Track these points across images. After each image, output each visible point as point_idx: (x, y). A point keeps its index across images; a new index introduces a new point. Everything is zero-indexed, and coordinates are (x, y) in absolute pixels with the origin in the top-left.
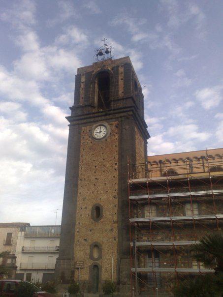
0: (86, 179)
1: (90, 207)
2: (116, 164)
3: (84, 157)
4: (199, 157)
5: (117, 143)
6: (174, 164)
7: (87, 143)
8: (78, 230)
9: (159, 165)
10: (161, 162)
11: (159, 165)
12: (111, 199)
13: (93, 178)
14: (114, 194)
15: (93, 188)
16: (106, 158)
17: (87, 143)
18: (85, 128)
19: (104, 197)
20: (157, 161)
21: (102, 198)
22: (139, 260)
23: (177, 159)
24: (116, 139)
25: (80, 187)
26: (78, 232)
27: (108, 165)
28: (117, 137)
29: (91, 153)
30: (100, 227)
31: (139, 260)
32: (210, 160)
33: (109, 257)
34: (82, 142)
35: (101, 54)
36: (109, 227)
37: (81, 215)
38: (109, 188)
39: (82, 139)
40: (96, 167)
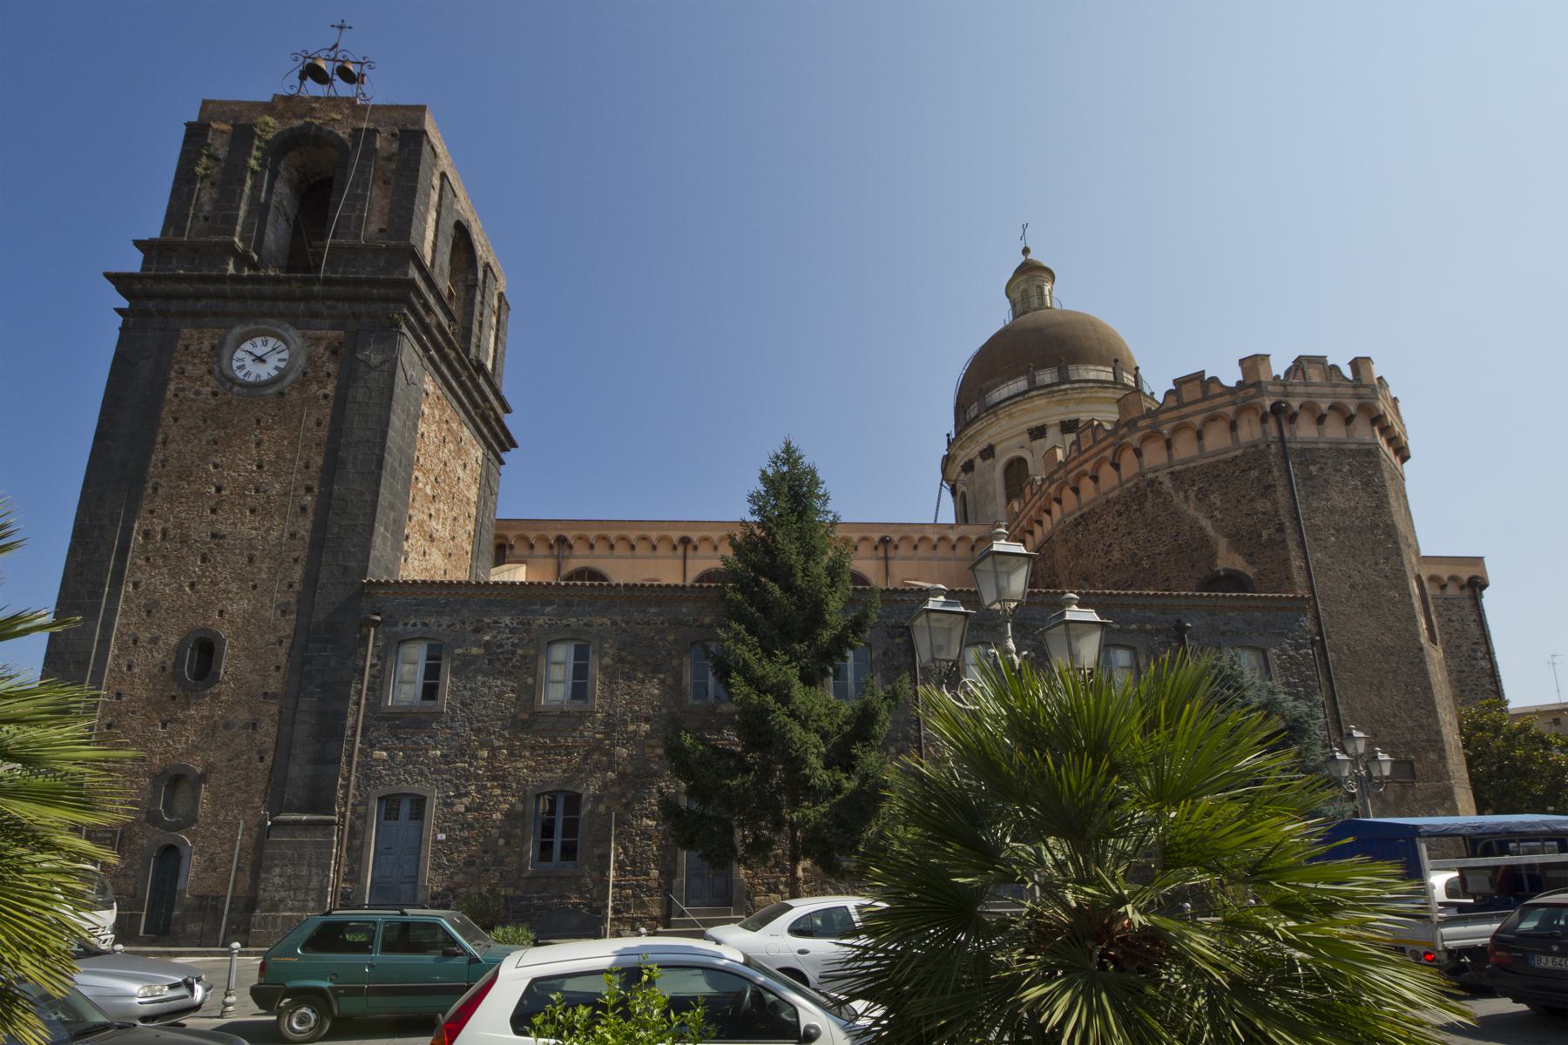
3: (173, 446)
7: (197, 393)
11: (555, 551)
17: (197, 393)
18: (196, 334)
24: (326, 396)
28: (330, 389)
40: (219, 490)
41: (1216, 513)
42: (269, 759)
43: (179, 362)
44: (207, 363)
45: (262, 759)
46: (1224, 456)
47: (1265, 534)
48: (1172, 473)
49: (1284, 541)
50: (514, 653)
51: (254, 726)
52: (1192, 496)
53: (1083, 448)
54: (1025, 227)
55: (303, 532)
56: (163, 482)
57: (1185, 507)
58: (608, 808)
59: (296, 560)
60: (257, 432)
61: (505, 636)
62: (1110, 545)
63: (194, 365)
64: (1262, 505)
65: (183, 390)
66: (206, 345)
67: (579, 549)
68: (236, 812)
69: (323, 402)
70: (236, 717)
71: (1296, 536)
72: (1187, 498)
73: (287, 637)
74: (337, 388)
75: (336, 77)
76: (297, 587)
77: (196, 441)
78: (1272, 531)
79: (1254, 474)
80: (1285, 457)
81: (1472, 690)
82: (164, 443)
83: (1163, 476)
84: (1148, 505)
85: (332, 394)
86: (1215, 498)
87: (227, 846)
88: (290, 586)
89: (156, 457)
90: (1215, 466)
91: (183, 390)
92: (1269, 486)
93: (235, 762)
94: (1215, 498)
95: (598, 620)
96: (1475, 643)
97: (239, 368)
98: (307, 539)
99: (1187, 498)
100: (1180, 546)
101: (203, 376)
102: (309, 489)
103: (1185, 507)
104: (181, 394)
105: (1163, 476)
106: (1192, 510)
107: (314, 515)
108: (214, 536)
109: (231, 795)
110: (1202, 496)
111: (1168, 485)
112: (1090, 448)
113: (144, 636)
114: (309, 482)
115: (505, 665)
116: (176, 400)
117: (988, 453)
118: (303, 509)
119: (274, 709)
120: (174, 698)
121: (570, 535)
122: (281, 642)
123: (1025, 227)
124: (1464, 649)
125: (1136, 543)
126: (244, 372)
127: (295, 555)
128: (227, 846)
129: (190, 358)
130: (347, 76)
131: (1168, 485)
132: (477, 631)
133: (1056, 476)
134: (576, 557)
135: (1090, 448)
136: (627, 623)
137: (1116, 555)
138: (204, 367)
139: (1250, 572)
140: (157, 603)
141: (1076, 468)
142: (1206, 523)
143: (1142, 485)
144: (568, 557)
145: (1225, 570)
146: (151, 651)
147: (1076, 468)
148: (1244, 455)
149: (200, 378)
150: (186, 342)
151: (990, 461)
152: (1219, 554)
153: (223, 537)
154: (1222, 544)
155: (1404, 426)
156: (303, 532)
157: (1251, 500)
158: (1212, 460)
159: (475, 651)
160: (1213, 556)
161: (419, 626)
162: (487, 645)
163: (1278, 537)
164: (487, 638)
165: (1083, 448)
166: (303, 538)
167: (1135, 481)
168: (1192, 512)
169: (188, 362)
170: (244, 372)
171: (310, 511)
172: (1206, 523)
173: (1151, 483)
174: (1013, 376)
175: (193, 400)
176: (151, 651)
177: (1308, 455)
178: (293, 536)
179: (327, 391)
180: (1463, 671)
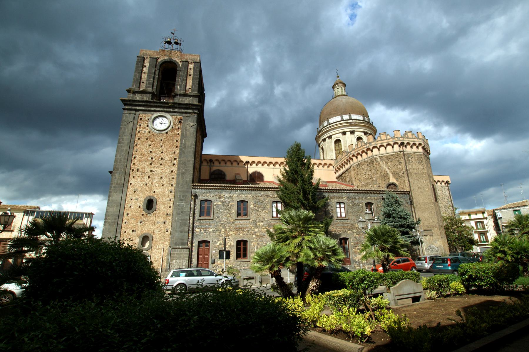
0: (140, 170)
1: (142, 199)
2: (175, 159)
3: (139, 146)
4: (208, 160)
5: (179, 138)
6: (223, 163)
7: (145, 132)
8: (125, 221)
9: (209, 164)
10: (211, 161)
11: (209, 164)
12: (167, 192)
13: (148, 170)
14: (170, 188)
15: (147, 180)
16: (165, 152)
17: (145, 132)
18: (144, 115)
19: (159, 190)
20: (208, 160)
21: (156, 191)
22: (306, 333)
23: (226, 160)
24: (178, 134)
25: (131, 177)
26: (125, 223)
27: (166, 159)
28: (179, 132)
29: (148, 144)
30: (152, 219)
31: (306, 333)
32: (216, 163)
33: (160, 247)
34: (138, 130)
35: (169, 43)
36: (162, 220)
37: (130, 207)
38: (165, 182)
39: (138, 126)
40: (152, 158)
41: (390, 168)
42: (169, 231)
43: (140, 123)
44: (147, 123)
45: (167, 231)
46: (391, 154)
47: (400, 174)
48: (380, 157)
49: (404, 176)
50: (229, 204)
51: (165, 223)
52: (384, 163)
53: (359, 147)
54: (337, 70)
55: (175, 171)
56: (137, 156)
57: (383, 165)
58: (254, 244)
59: (173, 178)
60: (161, 143)
61: (226, 200)
62: (366, 173)
63: (144, 124)
64: (399, 167)
65: (141, 131)
66: (147, 118)
67: (216, 163)
68: (161, 245)
69: (178, 135)
70: (160, 220)
71: (407, 175)
72: (383, 163)
73: (172, 199)
74: (181, 132)
75: (174, 44)
76: (174, 186)
77: (145, 145)
78: (402, 173)
79: (397, 159)
80: (404, 155)
81: (448, 210)
82: (136, 145)
83: (378, 157)
84: (375, 164)
85: (180, 133)
86: (389, 164)
87: (159, 255)
88: (172, 185)
89: (135, 149)
90: (389, 156)
91: (141, 131)
92: (400, 163)
93: (160, 232)
94: (389, 164)
95: (249, 196)
96: (448, 198)
97: (155, 125)
98: (176, 173)
99: (383, 163)
100: (382, 175)
101: (146, 127)
102: (175, 159)
103: (383, 165)
104: (140, 132)
105: (378, 157)
106: (384, 167)
107: (177, 166)
108: (151, 171)
109: (160, 241)
110: (386, 163)
111: (379, 160)
112: (360, 147)
113: (134, 198)
114: (175, 157)
115: (226, 207)
116: (139, 133)
117: (330, 137)
118: (174, 164)
119: (170, 218)
120: (143, 215)
121: (214, 159)
122: (170, 200)
123: (337, 70)
124: (446, 199)
125: (372, 173)
126: (157, 126)
127: (173, 177)
128: (159, 255)
129: (142, 122)
130: (176, 43)
131: (379, 160)
132: (220, 198)
133: (352, 152)
134: (215, 166)
135: (360, 147)
136: (256, 197)
137: (367, 176)
138: (146, 125)
139: (397, 183)
140: (137, 190)
141: (357, 151)
142: (387, 170)
143: (373, 159)
144: (213, 166)
145: (392, 182)
146: (136, 202)
147: (357, 151)
148: (395, 154)
149: (146, 128)
150: (141, 118)
151: (330, 140)
152: (391, 178)
153: (154, 171)
154: (391, 176)
155: (429, 146)
156: (175, 171)
157: (397, 165)
158: (388, 154)
159: (219, 203)
160: (389, 178)
161: (205, 196)
162: (222, 202)
163: (403, 175)
164: (222, 200)
165: (359, 147)
166: (174, 172)
167: (371, 157)
168: (385, 167)
169: (142, 123)
170: (157, 126)
171: (176, 165)
172: (387, 170)
173: (375, 159)
174: (336, 115)
175: (144, 134)
176: (136, 202)
177: (409, 155)
178: (172, 171)
179: (179, 133)
180: (445, 205)
